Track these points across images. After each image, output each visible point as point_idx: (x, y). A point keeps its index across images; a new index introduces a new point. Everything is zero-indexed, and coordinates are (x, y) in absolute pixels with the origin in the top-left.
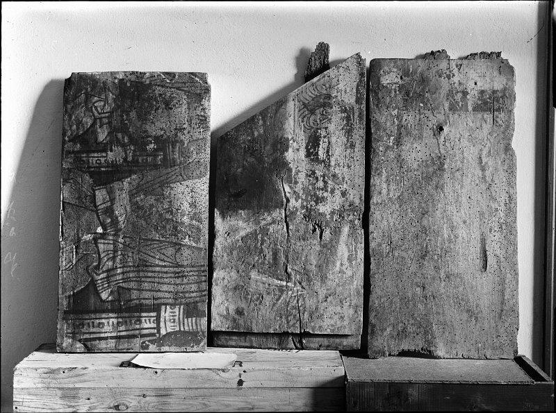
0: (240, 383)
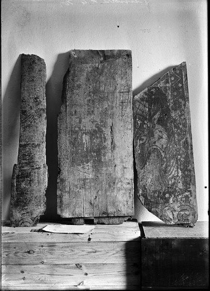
0: (89, 239)
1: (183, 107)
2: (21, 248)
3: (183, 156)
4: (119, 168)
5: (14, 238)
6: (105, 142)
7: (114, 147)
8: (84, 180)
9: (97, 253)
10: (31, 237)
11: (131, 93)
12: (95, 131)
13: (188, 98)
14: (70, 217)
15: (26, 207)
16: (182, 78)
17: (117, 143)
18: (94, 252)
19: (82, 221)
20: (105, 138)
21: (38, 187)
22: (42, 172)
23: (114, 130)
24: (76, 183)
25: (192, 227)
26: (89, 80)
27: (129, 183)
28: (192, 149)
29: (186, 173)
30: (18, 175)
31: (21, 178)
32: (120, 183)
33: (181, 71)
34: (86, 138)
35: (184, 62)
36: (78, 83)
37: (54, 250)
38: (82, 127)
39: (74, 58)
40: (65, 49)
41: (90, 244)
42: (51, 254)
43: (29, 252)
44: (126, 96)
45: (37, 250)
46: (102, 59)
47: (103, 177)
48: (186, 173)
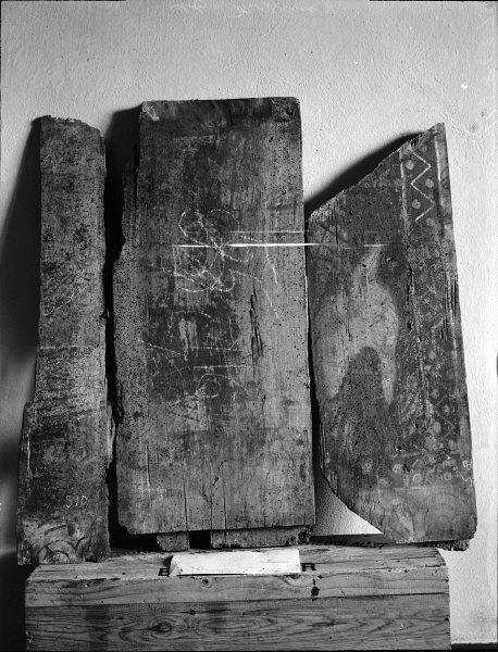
0: (315, 591)
1: (437, 238)
2: (138, 618)
3: (439, 366)
4: (273, 405)
5: (118, 591)
6: (236, 338)
7: (259, 348)
8: (186, 436)
9: (336, 627)
10: (162, 589)
11: (301, 210)
12: (210, 309)
13: (449, 216)
14: (152, 531)
15: (56, 514)
16: (434, 165)
17: (268, 342)
18: (329, 625)
19: (185, 542)
20: (236, 328)
21: (87, 462)
22: (97, 421)
23: (258, 306)
24: (164, 445)
25: (462, 550)
26: (191, 177)
27: (300, 442)
28: (460, 348)
29: (447, 409)
30: (37, 431)
31: (44, 437)
32: (277, 443)
33: (429, 144)
34: (186, 329)
35: (441, 126)
36: (164, 186)
37: (224, 621)
38: (176, 300)
39: (152, 123)
40: (128, 103)
41: (317, 603)
42: (216, 631)
43: (158, 629)
44: (287, 215)
45: (179, 622)
46: (224, 123)
47: (234, 428)
48: (447, 409)
